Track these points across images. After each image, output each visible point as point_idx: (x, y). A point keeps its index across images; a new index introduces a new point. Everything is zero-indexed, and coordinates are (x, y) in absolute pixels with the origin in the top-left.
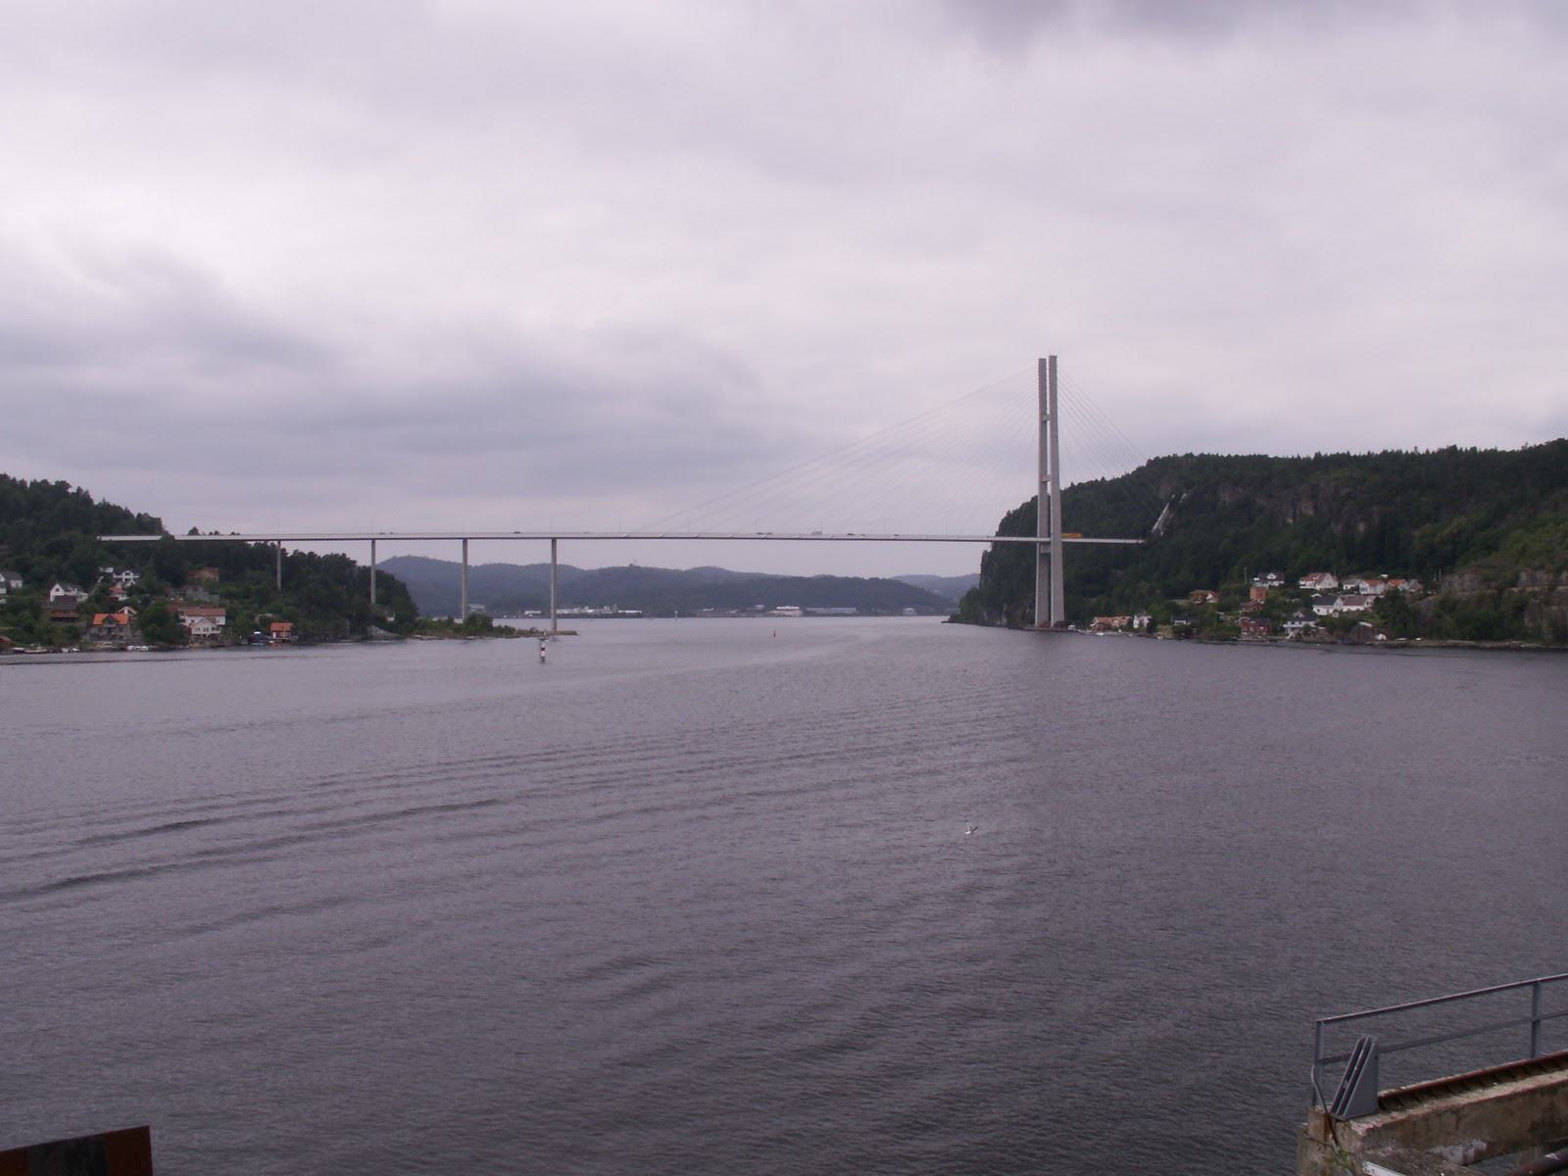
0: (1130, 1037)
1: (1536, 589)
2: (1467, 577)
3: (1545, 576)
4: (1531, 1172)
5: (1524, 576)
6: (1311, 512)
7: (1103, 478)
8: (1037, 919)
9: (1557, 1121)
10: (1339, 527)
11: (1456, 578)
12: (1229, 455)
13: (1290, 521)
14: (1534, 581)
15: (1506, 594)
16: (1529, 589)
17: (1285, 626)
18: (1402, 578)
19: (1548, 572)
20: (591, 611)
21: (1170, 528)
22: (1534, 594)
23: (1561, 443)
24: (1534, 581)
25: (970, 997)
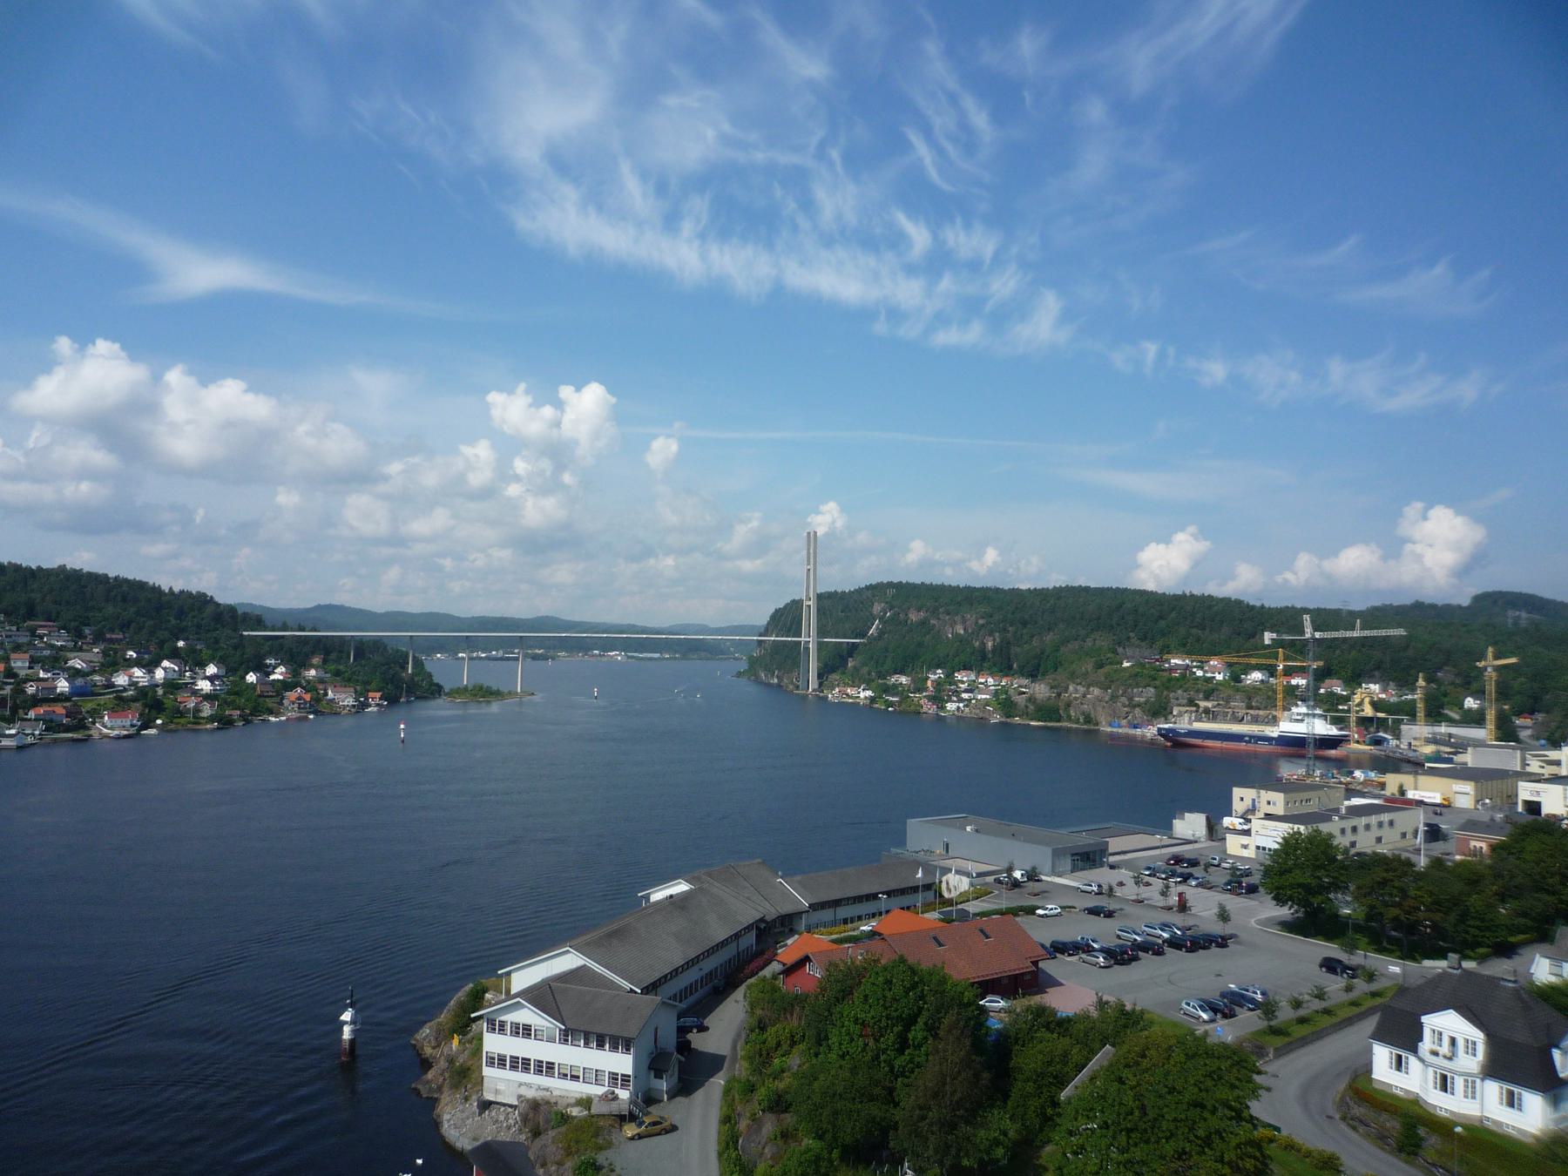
0: (778, 1104)
1: (1077, 696)
2: (1042, 686)
3: (1082, 689)
4: (1000, 1152)
5: (1071, 688)
6: (962, 632)
7: (171, 588)
8: (841, 959)
9: (1538, 877)
10: (978, 643)
11: (1037, 685)
12: (932, 584)
13: (950, 636)
14: (1076, 691)
15: (1062, 697)
16: (1074, 695)
17: (1480, 664)
18: (1255, 670)
19: (1084, 687)
20: (483, 655)
21: (881, 633)
22: (1076, 698)
23: (1562, 604)
24: (1076, 691)
25: (556, 1131)
